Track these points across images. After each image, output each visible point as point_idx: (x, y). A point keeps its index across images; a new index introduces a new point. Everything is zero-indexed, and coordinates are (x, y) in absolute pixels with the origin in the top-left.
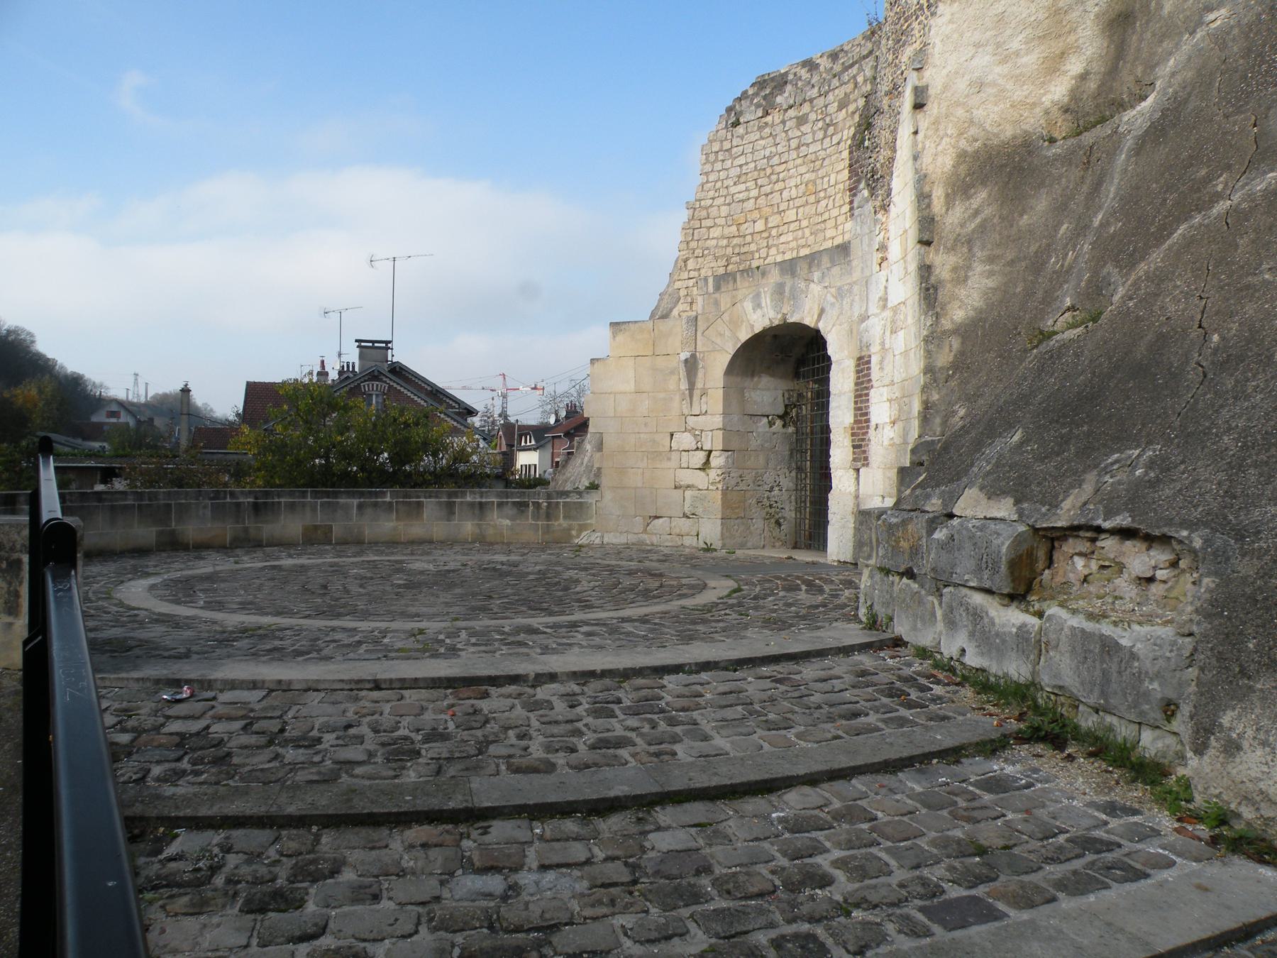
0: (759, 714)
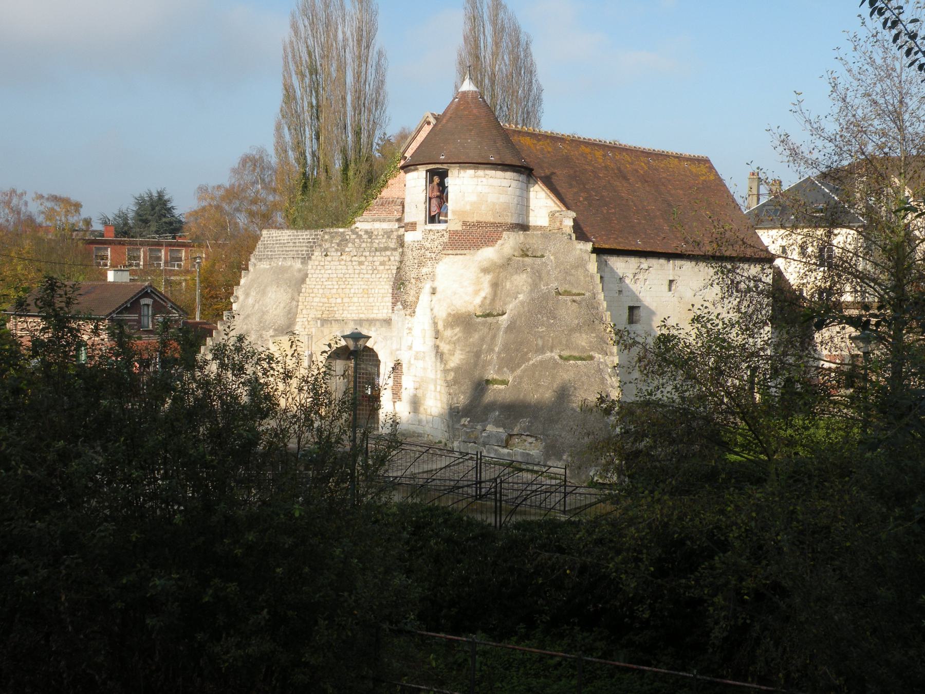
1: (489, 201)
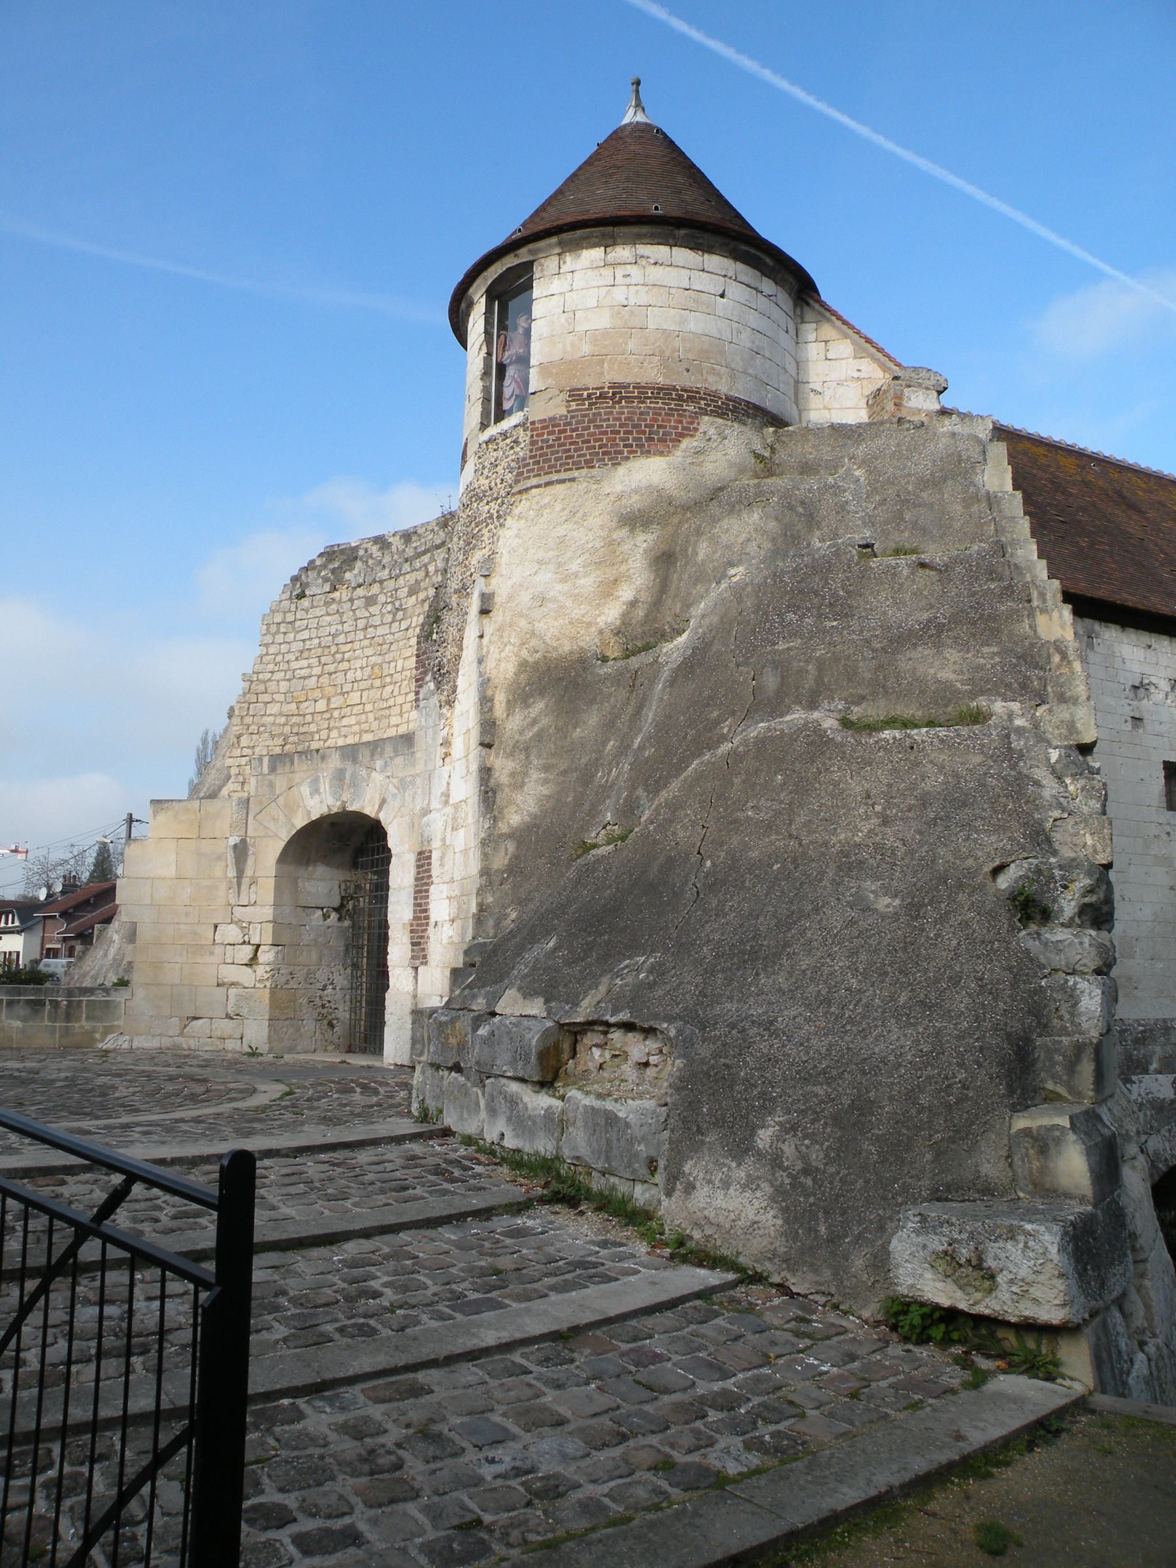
0: (319, 1190)
1: (651, 326)
